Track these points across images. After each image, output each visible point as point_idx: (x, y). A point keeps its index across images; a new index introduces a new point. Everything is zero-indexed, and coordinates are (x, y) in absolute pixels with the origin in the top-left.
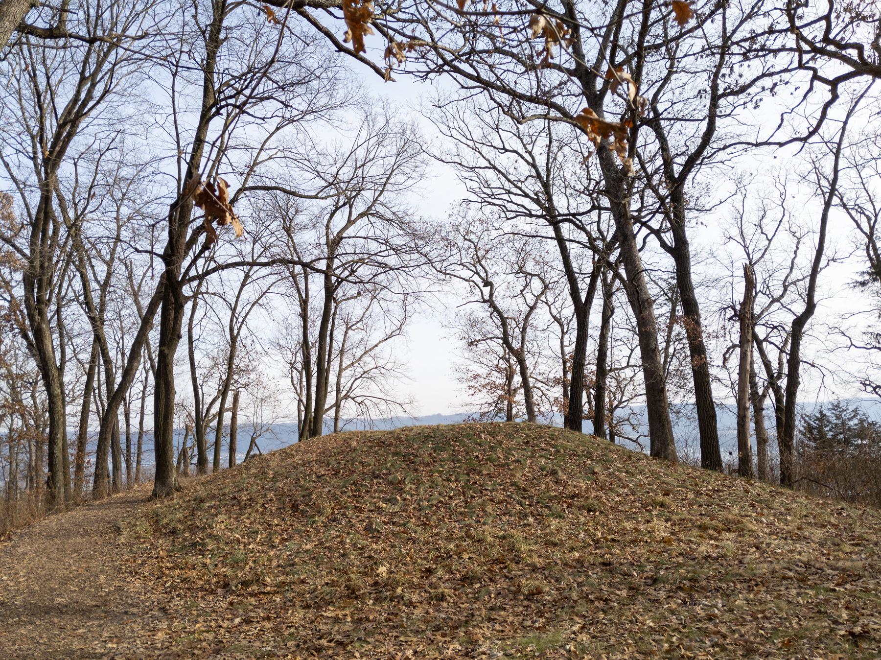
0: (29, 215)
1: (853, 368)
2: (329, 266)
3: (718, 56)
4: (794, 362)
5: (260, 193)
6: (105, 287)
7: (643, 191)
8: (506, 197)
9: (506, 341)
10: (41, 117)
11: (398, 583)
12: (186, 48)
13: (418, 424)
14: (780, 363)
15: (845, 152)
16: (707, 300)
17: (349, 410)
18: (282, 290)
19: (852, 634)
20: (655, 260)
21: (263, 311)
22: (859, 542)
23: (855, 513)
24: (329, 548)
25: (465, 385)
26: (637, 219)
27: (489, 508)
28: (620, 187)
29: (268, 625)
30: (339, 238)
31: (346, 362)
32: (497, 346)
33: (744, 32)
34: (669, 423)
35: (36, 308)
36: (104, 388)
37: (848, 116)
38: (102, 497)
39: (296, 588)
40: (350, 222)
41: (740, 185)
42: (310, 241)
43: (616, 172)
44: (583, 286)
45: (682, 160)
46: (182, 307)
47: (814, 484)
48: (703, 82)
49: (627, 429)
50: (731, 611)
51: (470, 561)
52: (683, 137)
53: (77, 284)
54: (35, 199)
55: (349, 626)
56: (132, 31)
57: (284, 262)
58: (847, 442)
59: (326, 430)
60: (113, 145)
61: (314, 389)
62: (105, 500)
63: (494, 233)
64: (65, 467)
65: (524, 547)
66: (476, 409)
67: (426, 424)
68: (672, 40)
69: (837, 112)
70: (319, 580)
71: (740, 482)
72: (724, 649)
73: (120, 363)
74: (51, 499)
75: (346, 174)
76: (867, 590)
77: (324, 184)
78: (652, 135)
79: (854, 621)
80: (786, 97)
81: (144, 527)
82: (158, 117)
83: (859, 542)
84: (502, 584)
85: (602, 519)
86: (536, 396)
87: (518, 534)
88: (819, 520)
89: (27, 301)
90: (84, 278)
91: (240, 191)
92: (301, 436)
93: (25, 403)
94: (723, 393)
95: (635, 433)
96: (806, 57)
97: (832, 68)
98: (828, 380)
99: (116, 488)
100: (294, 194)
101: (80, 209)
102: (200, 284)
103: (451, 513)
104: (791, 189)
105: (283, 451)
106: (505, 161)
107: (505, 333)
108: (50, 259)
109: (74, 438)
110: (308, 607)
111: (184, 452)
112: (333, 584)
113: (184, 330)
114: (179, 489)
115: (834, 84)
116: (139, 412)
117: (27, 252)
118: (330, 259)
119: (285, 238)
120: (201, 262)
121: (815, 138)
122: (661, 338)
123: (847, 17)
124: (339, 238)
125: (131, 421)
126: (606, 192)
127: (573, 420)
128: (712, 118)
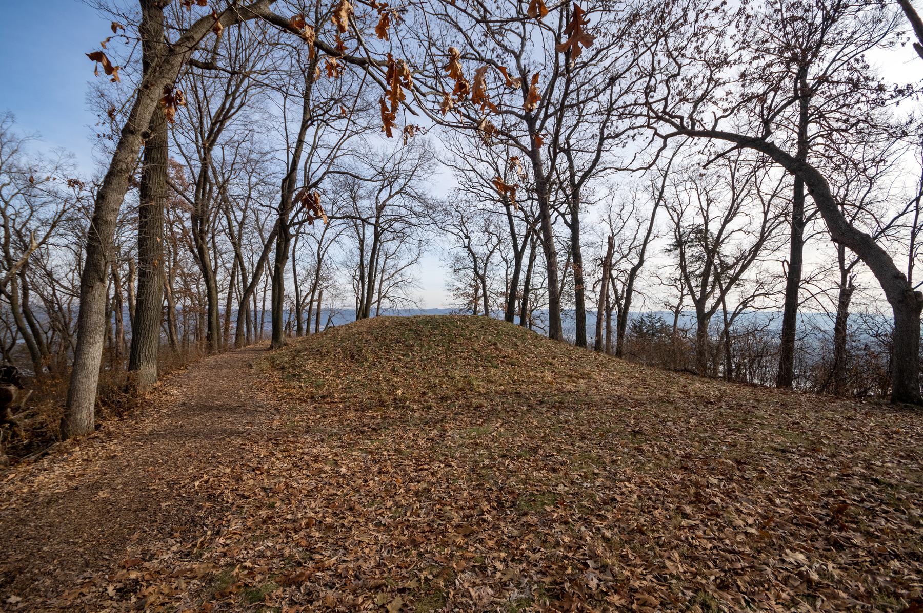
0: (194, 178)
1: (661, 296)
2: (377, 221)
3: (605, 116)
4: (630, 291)
5: (338, 175)
6: (241, 224)
7: (557, 191)
8: (480, 188)
9: (476, 271)
10: (201, 117)
11: (407, 399)
12: (293, 82)
13: (424, 314)
14: (623, 292)
15: (670, 176)
16: (588, 255)
17: (386, 304)
18: (349, 233)
19: (634, 431)
20: (561, 230)
21: (337, 245)
22: (647, 386)
23: (649, 372)
24: (371, 380)
25: (452, 294)
26: (552, 207)
27: (459, 362)
28: (544, 188)
29: (335, 419)
30: (384, 205)
31: (385, 277)
32: (471, 273)
33: (620, 103)
34: (560, 320)
35: (200, 236)
36: (241, 284)
37: (673, 156)
38: (240, 347)
39: (351, 400)
40: (390, 196)
41: (611, 190)
42: (366, 205)
43: (543, 178)
44: (520, 242)
45: (580, 174)
46: (289, 240)
47: (633, 356)
48: (596, 129)
49: (538, 322)
50: (577, 418)
51: (447, 389)
52: (582, 161)
53: (224, 222)
54: (197, 171)
55: (379, 421)
56: (259, 67)
57: (350, 217)
58: (653, 335)
59: (372, 315)
60: (247, 139)
61: (366, 291)
62: (242, 349)
63: (473, 209)
64: (218, 329)
65: (475, 383)
66: (457, 307)
67: (428, 314)
68: (581, 103)
69: (668, 153)
70: (365, 397)
71: (594, 354)
72: (570, 437)
73: (250, 271)
74: (210, 347)
75: (389, 167)
76: (646, 410)
77: (376, 172)
78: (565, 158)
79: (636, 425)
80: (641, 142)
81: (265, 365)
82: (275, 124)
83: (647, 386)
84: (462, 401)
85: (518, 370)
86: (490, 301)
87: (473, 376)
88: (630, 375)
89: (194, 230)
90: (228, 218)
91: (325, 174)
92: (357, 317)
93: (193, 291)
94: (590, 305)
95: (542, 326)
96: (652, 121)
97: (665, 128)
98: (647, 302)
99: (248, 343)
100: (358, 177)
101: (226, 176)
102: (300, 227)
103: (438, 363)
104: (639, 195)
105: (347, 325)
106: (481, 167)
107: (476, 265)
108: (208, 207)
109: (223, 313)
110: (357, 410)
111: (289, 324)
112: (372, 398)
113: (290, 253)
114: (286, 344)
115: (665, 138)
116: (263, 299)
117: (193, 200)
118: (378, 217)
119: (352, 203)
120: (300, 215)
121: (654, 167)
122: (560, 274)
123: (678, 99)
124: (384, 205)
125: (258, 305)
126: (537, 191)
127: (509, 316)
128: (599, 151)
